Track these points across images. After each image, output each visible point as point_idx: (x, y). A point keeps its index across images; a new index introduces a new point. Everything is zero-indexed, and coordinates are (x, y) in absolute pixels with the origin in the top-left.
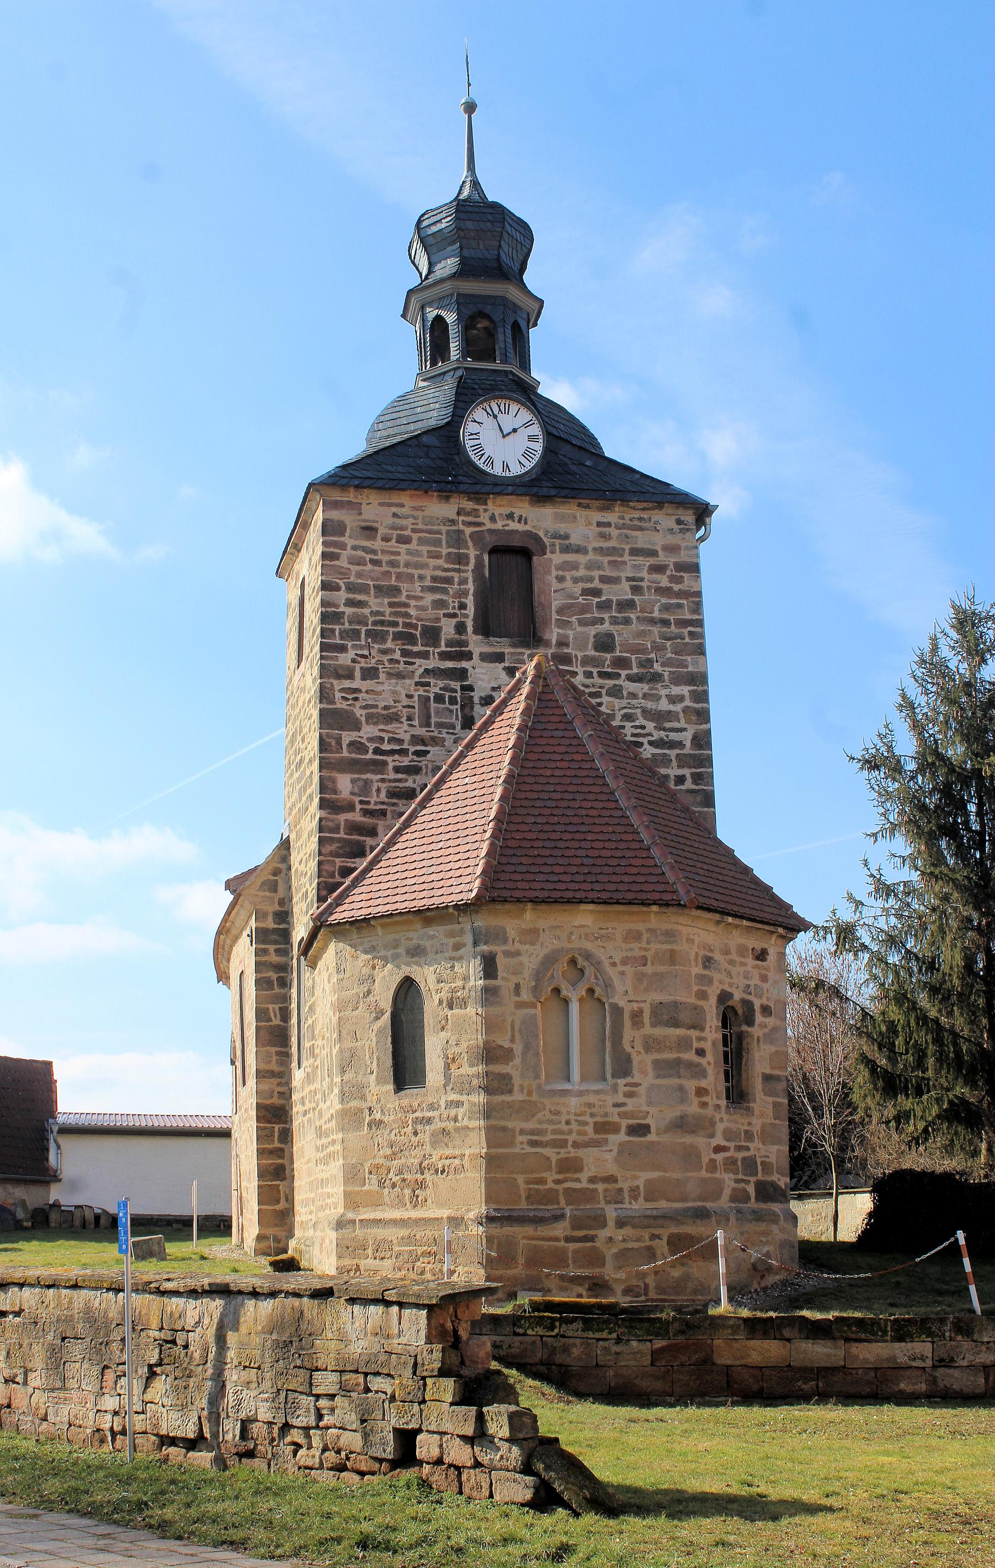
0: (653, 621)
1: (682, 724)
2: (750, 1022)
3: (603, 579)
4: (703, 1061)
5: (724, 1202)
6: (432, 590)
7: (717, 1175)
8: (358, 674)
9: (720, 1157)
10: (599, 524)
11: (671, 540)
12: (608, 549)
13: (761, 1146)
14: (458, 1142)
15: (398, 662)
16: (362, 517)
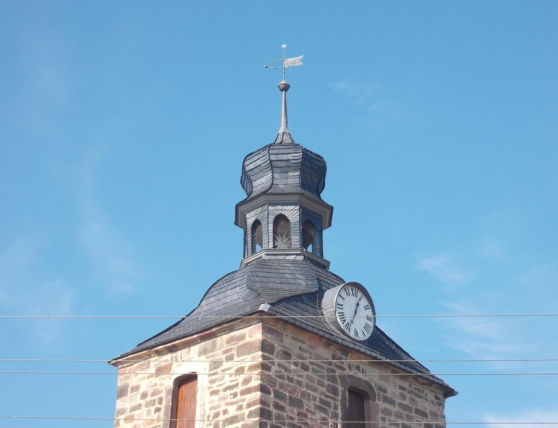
10: (401, 387)
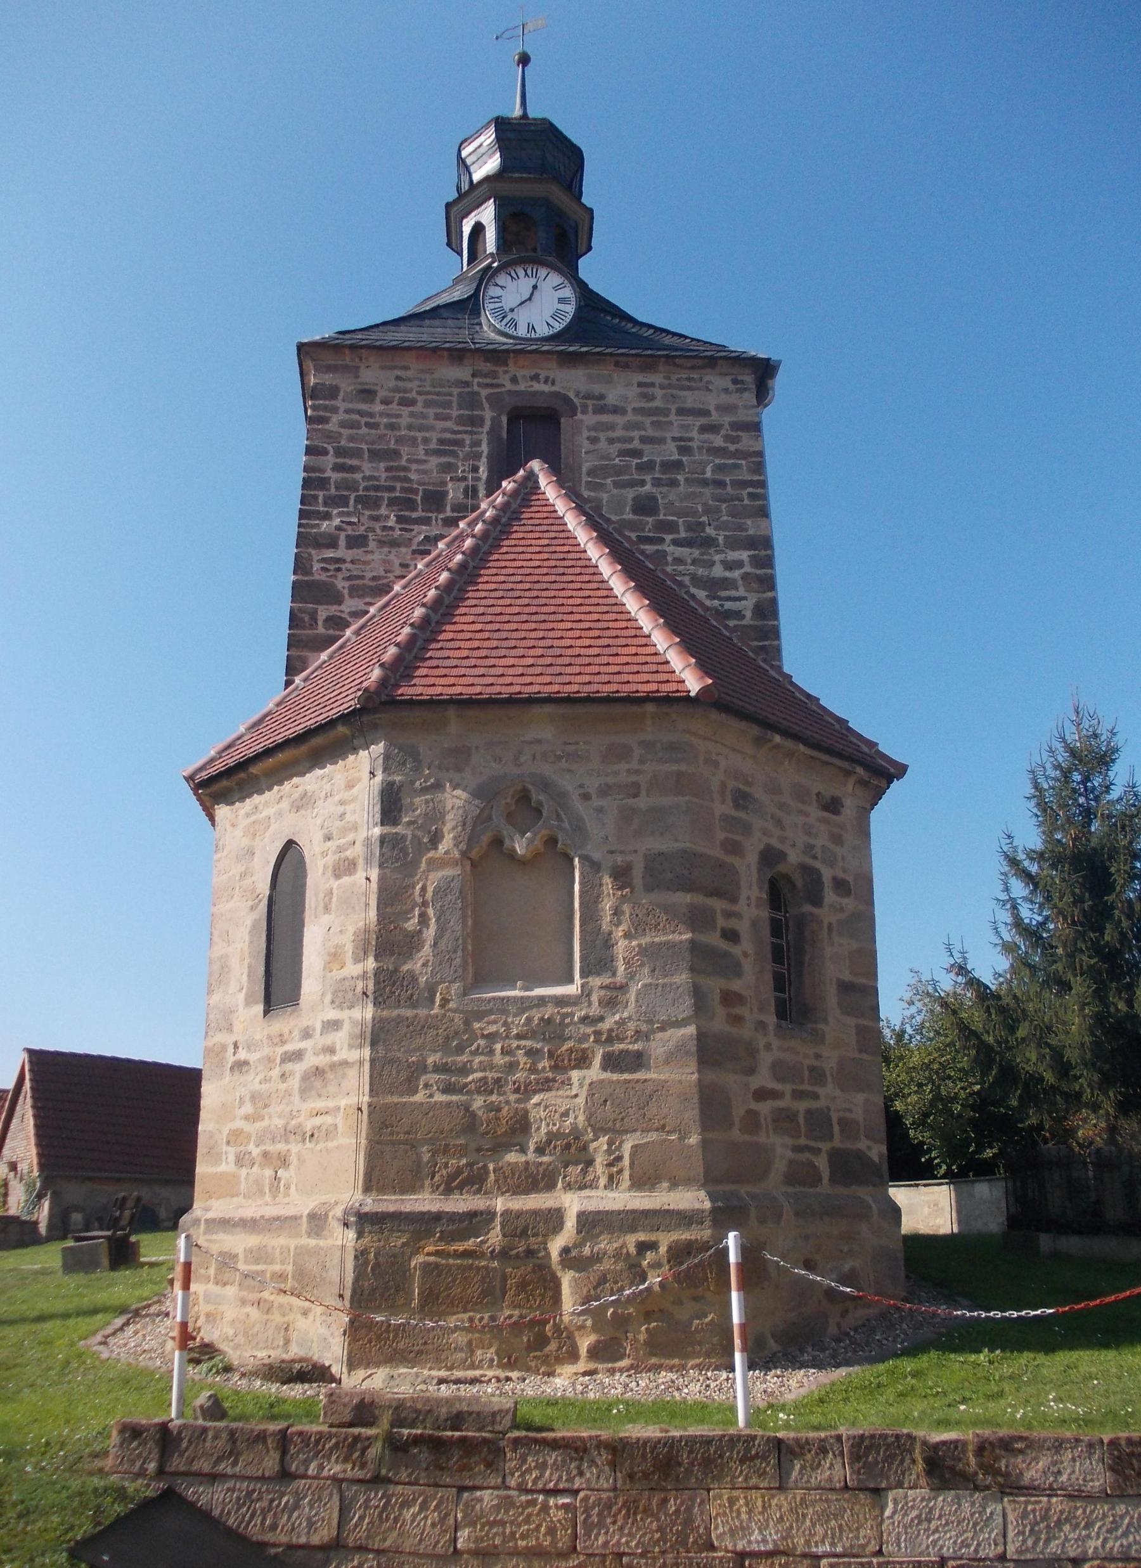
0: (705, 483)
1: (741, 592)
2: (817, 901)
3: (644, 440)
4: (736, 950)
5: (774, 1183)
6: (438, 453)
7: (762, 1138)
8: (342, 542)
9: (765, 1108)
10: (640, 385)
11: (725, 399)
12: (650, 409)
13: (838, 1092)
14: (332, 1088)
15: (392, 529)
16: (359, 380)
